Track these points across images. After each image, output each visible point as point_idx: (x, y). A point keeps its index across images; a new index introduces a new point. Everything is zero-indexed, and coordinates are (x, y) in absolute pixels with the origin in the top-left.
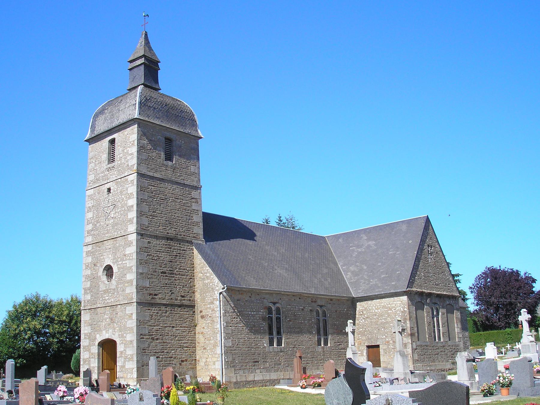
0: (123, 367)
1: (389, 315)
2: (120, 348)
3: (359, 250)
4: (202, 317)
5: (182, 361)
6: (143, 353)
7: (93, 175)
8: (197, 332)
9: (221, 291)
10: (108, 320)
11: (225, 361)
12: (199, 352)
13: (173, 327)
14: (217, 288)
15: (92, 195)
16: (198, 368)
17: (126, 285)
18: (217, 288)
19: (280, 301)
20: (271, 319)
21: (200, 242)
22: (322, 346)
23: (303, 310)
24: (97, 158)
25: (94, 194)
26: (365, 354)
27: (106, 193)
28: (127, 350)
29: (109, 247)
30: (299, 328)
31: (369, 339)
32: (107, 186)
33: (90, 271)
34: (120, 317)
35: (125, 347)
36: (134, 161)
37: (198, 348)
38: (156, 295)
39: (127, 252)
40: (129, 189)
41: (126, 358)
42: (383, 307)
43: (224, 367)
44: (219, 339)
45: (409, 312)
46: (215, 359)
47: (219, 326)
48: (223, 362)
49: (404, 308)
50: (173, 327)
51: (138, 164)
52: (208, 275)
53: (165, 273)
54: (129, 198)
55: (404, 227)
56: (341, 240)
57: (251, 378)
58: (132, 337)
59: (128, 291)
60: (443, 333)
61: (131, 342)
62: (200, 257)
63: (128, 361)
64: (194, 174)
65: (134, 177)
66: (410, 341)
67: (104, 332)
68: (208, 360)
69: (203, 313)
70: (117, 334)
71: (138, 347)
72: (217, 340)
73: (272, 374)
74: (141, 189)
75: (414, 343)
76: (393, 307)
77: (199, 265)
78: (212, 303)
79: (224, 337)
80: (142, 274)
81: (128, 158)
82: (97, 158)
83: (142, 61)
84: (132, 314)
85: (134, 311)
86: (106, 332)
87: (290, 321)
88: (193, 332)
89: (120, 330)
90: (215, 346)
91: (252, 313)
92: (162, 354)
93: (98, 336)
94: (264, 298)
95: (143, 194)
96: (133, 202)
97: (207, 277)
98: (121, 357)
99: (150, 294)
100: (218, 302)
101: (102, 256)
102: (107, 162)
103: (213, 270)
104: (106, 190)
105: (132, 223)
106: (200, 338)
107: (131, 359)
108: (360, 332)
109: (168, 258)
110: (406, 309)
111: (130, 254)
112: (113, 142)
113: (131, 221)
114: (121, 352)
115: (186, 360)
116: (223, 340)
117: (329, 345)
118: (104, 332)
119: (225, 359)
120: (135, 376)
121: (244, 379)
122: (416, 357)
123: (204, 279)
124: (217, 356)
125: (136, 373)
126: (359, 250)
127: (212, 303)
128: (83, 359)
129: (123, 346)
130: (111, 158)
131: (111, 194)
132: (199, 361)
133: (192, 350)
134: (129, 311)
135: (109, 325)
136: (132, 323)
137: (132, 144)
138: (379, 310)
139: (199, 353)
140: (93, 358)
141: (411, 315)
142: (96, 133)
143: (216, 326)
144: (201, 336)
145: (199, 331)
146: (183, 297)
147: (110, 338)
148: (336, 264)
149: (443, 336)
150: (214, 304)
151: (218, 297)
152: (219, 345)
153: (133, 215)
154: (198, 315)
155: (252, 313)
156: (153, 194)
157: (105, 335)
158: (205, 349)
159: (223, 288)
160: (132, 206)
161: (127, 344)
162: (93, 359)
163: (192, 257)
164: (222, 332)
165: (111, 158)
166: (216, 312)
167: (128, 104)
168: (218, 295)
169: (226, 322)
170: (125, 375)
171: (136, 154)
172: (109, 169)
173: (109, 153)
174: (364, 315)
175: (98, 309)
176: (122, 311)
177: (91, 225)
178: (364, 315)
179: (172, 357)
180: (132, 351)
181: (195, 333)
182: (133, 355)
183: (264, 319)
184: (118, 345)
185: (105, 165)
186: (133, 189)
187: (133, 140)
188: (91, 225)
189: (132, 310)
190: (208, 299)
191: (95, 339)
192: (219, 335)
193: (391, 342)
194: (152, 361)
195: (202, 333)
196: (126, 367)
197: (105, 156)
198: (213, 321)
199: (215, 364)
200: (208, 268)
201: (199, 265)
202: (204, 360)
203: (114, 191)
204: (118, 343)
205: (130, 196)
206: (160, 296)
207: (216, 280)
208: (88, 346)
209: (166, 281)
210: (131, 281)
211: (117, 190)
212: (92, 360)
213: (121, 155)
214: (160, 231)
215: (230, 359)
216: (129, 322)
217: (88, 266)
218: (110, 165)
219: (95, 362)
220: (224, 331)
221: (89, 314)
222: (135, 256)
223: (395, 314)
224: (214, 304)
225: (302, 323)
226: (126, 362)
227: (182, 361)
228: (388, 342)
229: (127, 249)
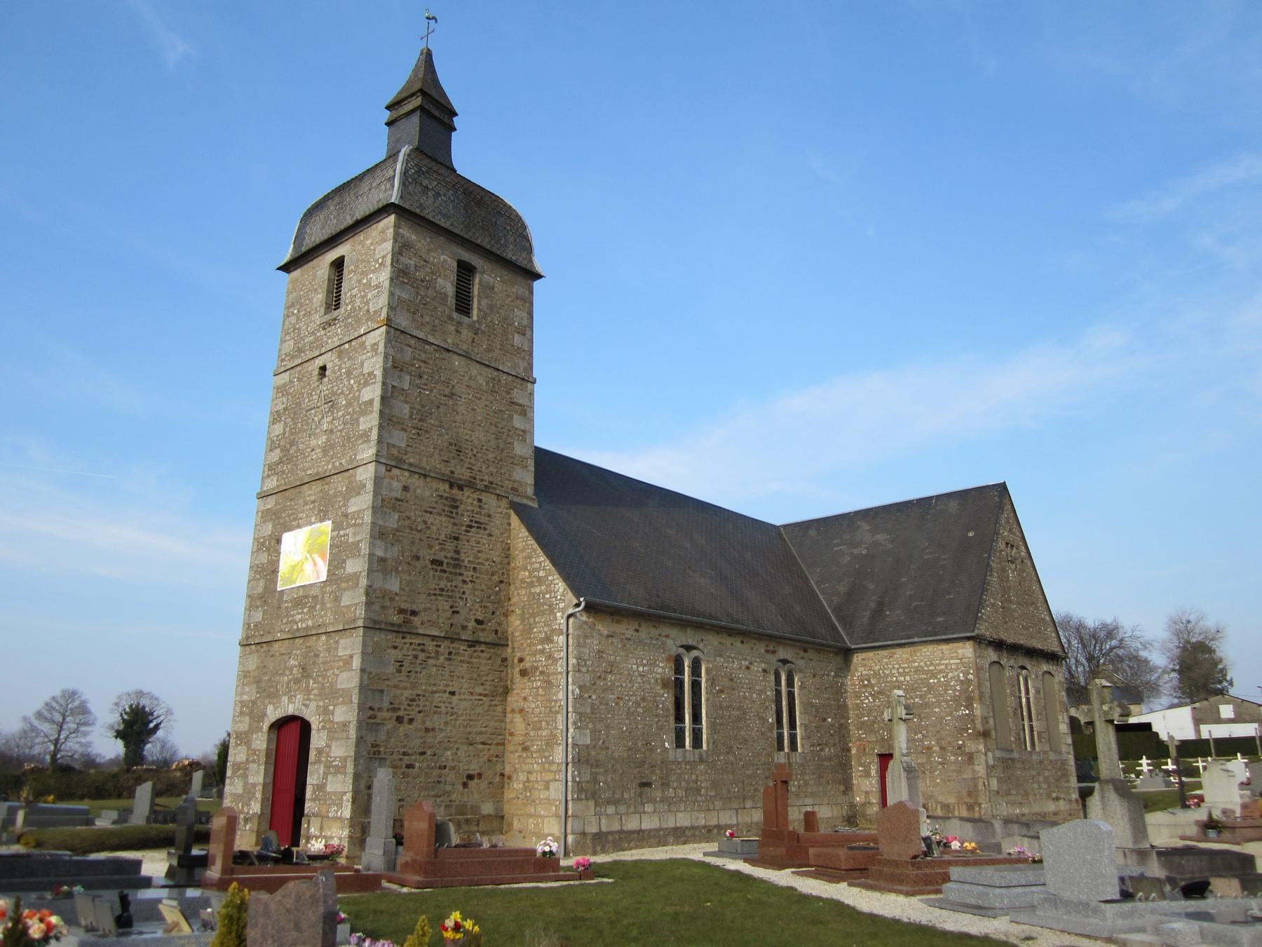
0: (321, 787)
1: (931, 688)
2: (317, 740)
3: (856, 552)
4: (524, 673)
5: (470, 777)
6: (370, 754)
7: (292, 342)
8: (509, 709)
9: (571, 611)
10: (295, 671)
11: (574, 781)
12: (511, 756)
13: (453, 693)
14: (562, 605)
15: (284, 385)
16: (509, 795)
17: (344, 585)
18: (562, 605)
19: (701, 646)
20: (679, 684)
21: (525, 501)
22: (786, 750)
23: (748, 668)
24: (302, 305)
25: (291, 381)
26: (873, 773)
27: (315, 378)
28: (334, 744)
29: (313, 498)
30: (739, 709)
31: (883, 739)
32: (319, 362)
33: (266, 554)
34: (324, 663)
35: (330, 738)
36: (383, 300)
37: (510, 748)
38: (414, 613)
39: (352, 509)
40: (366, 365)
41: (328, 766)
42: (917, 670)
43: (569, 798)
44: (561, 726)
45: (980, 685)
46: (549, 776)
47: (561, 695)
48: (570, 784)
49: (966, 674)
50: (453, 693)
51: (392, 308)
52: (542, 574)
53: (441, 563)
54: (366, 384)
55: (953, 506)
56: (812, 533)
57: (632, 824)
58: (346, 714)
59: (346, 600)
60: (1039, 733)
61: (345, 725)
62: (524, 533)
63: (335, 774)
64: (519, 350)
65: (379, 336)
66: (982, 747)
67: (285, 699)
68: (532, 778)
69: (527, 664)
70: (313, 705)
71: (360, 740)
72: (556, 728)
73: (680, 815)
74: (394, 367)
75: (990, 754)
76: (941, 671)
77: (522, 551)
78: (548, 639)
79: (575, 723)
80: (382, 560)
81: (369, 296)
82: (302, 305)
83: (417, 101)
84: (351, 657)
85: (358, 650)
86: (290, 701)
87: (721, 691)
88: (499, 709)
89: (322, 695)
90: (550, 743)
91: (641, 669)
92: (422, 758)
93: (270, 708)
94: (667, 636)
95: (400, 377)
96: (373, 393)
97: (539, 578)
98: (318, 762)
99: (401, 611)
100: (562, 639)
101: (295, 519)
102: (323, 310)
103: (554, 563)
104: (316, 372)
105: (369, 441)
106: (518, 724)
107: (339, 770)
108: (863, 723)
109: (448, 529)
110: (970, 677)
111: (359, 512)
112: (338, 264)
113: (365, 436)
114: (320, 751)
115: (480, 775)
116: (571, 730)
117: (800, 750)
118: (285, 699)
119: (573, 777)
120: (347, 812)
121: (616, 827)
122: (994, 784)
123: (531, 585)
124: (554, 768)
125: (349, 804)
126: (856, 552)
127: (548, 639)
128: (234, 765)
129: (324, 734)
130: (334, 300)
131: (326, 380)
132: (510, 778)
133: (494, 750)
134: (345, 648)
135: (297, 681)
136: (349, 680)
137: (381, 264)
138: (908, 678)
139: (513, 758)
140: (254, 761)
141: (983, 689)
142: (304, 249)
143: (556, 694)
144: (518, 719)
145: (515, 706)
146: (479, 622)
147: (297, 713)
148: (806, 581)
149: (1040, 741)
150: (552, 642)
151: (564, 627)
152: (561, 740)
153: (370, 422)
154: (512, 667)
155: (641, 669)
156: (424, 381)
157: (290, 708)
158: (526, 749)
159: (577, 605)
160: (371, 402)
161: (335, 731)
162: (255, 766)
163: (502, 577)
164: (570, 709)
165: (334, 300)
166: (557, 660)
167: (378, 181)
168: (563, 621)
169: (580, 687)
170: (324, 809)
171: (387, 284)
172: (328, 324)
173: (329, 292)
174: (872, 686)
175: (276, 646)
176: (328, 650)
177: (278, 451)
178: (872, 686)
179: (445, 767)
180: (342, 750)
181: (504, 713)
182: (346, 758)
183: (665, 685)
184: (313, 733)
185: (318, 318)
186: (374, 365)
187: (382, 254)
188: (278, 451)
189: (351, 647)
190: (539, 631)
191: (264, 715)
192: (560, 718)
193: (936, 748)
194: (152, 725)
195: (521, 711)
196: (329, 789)
197: (319, 298)
198: (549, 682)
199: (547, 788)
200: (543, 558)
201: (522, 551)
202: (523, 777)
203: (334, 372)
204: (314, 727)
205: (367, 380)
206: (424, 616)
207: (561, 586)
208: (246, 733)
209: (443, 584)
210: (355, 577)
211: (340, 369)
212: (253, 766)
213: (355, 291)
214: (434, 463)
215: (587, 777)
216: (345, 675)
217: (263, 544)
218: (328, 317)
219: (258, 772)
220: (574, 707)
221: (255, 656)
222: (368, 518)
223: (947, 686)
224: (552, 642)
225: (745, 698)
226: (330, 777)
227: (470, 777)
228: (929, 748)
229: (353, 500)
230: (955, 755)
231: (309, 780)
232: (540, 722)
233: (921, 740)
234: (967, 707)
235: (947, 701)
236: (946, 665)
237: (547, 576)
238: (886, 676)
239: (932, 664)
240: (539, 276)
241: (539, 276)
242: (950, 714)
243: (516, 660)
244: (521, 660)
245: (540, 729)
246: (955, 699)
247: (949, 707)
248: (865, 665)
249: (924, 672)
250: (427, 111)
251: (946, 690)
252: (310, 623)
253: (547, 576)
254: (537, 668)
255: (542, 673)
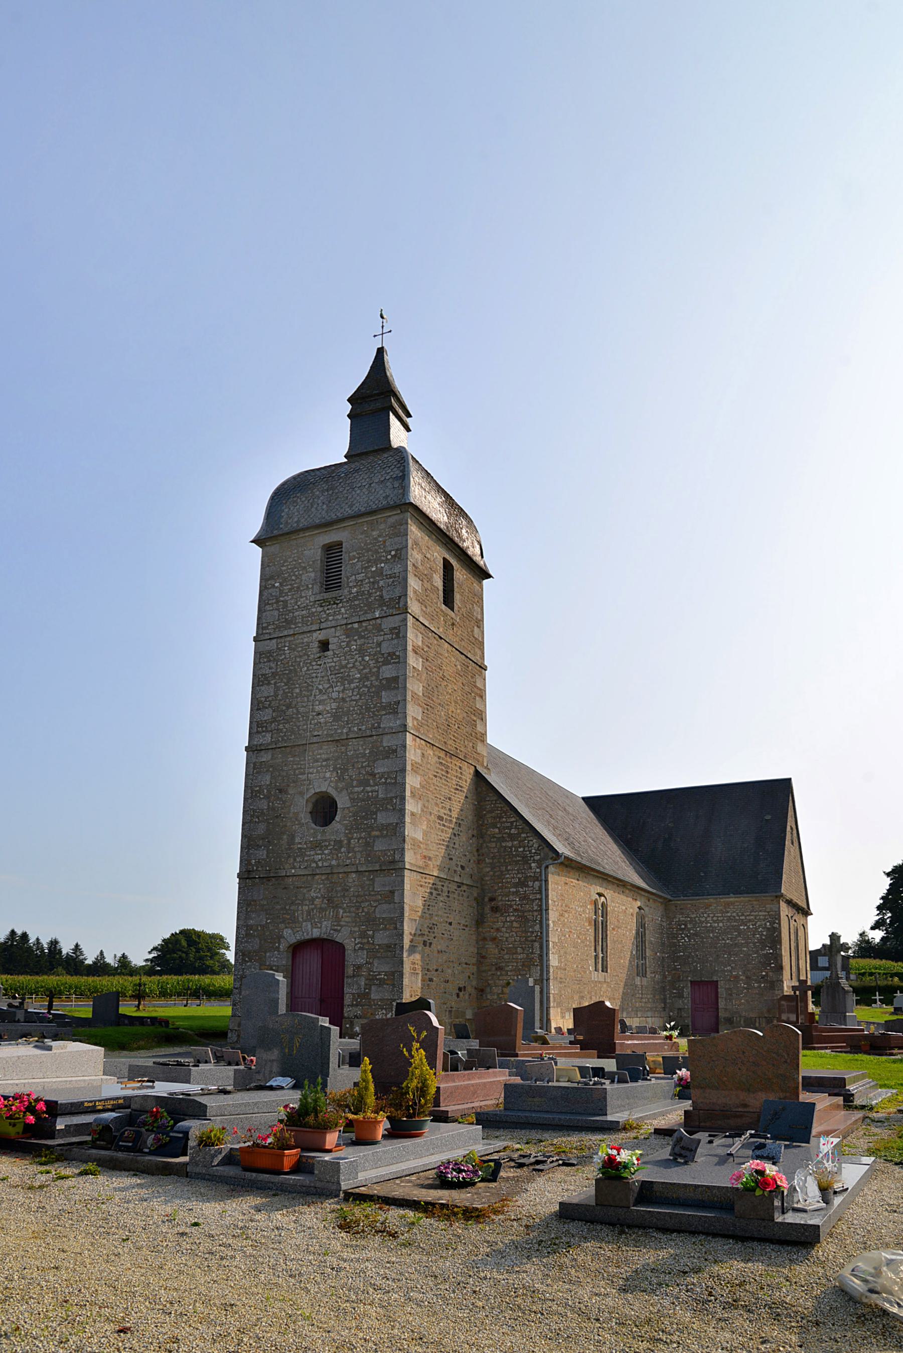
1: (740, 933)
4: (495, 910)
5: (460, 989)
32: (321, 636)
42: (729, 919)
55: (267, 691)
76: (750, 921)
81: (381, 583)
97: (510, 835)
158: (500, 969)
174: (689, 930)
178: (689, 930)
201: (491, 812)
228: (736, 977)
229: (380, 762)
230: (760, 982)
231: (346, 990)
232: (516, 948)
233: (730, 971)
234: (771, 948)
235: (754, 943)
236: (756, 916)
237: (519, 834)
238: (702, 922)
239: (743, 915)
240: (489, 576)
241: (489, 576)
242: (757, 952)
243: (486, 899)
244: (492, 899)
245: (516, 953)
246: (761, 941)
247: (755, 947)
248: (682, 914)
249: (736, 921)
250: (375, 401)
251: (754, 935)
252: (334, 862)
253: (519, 834)
254: (511, 906)
255: (516, 910)
